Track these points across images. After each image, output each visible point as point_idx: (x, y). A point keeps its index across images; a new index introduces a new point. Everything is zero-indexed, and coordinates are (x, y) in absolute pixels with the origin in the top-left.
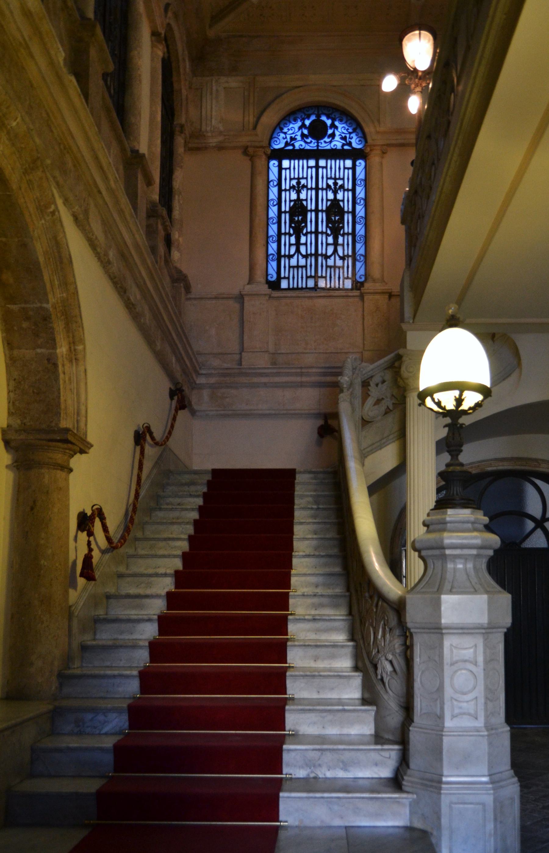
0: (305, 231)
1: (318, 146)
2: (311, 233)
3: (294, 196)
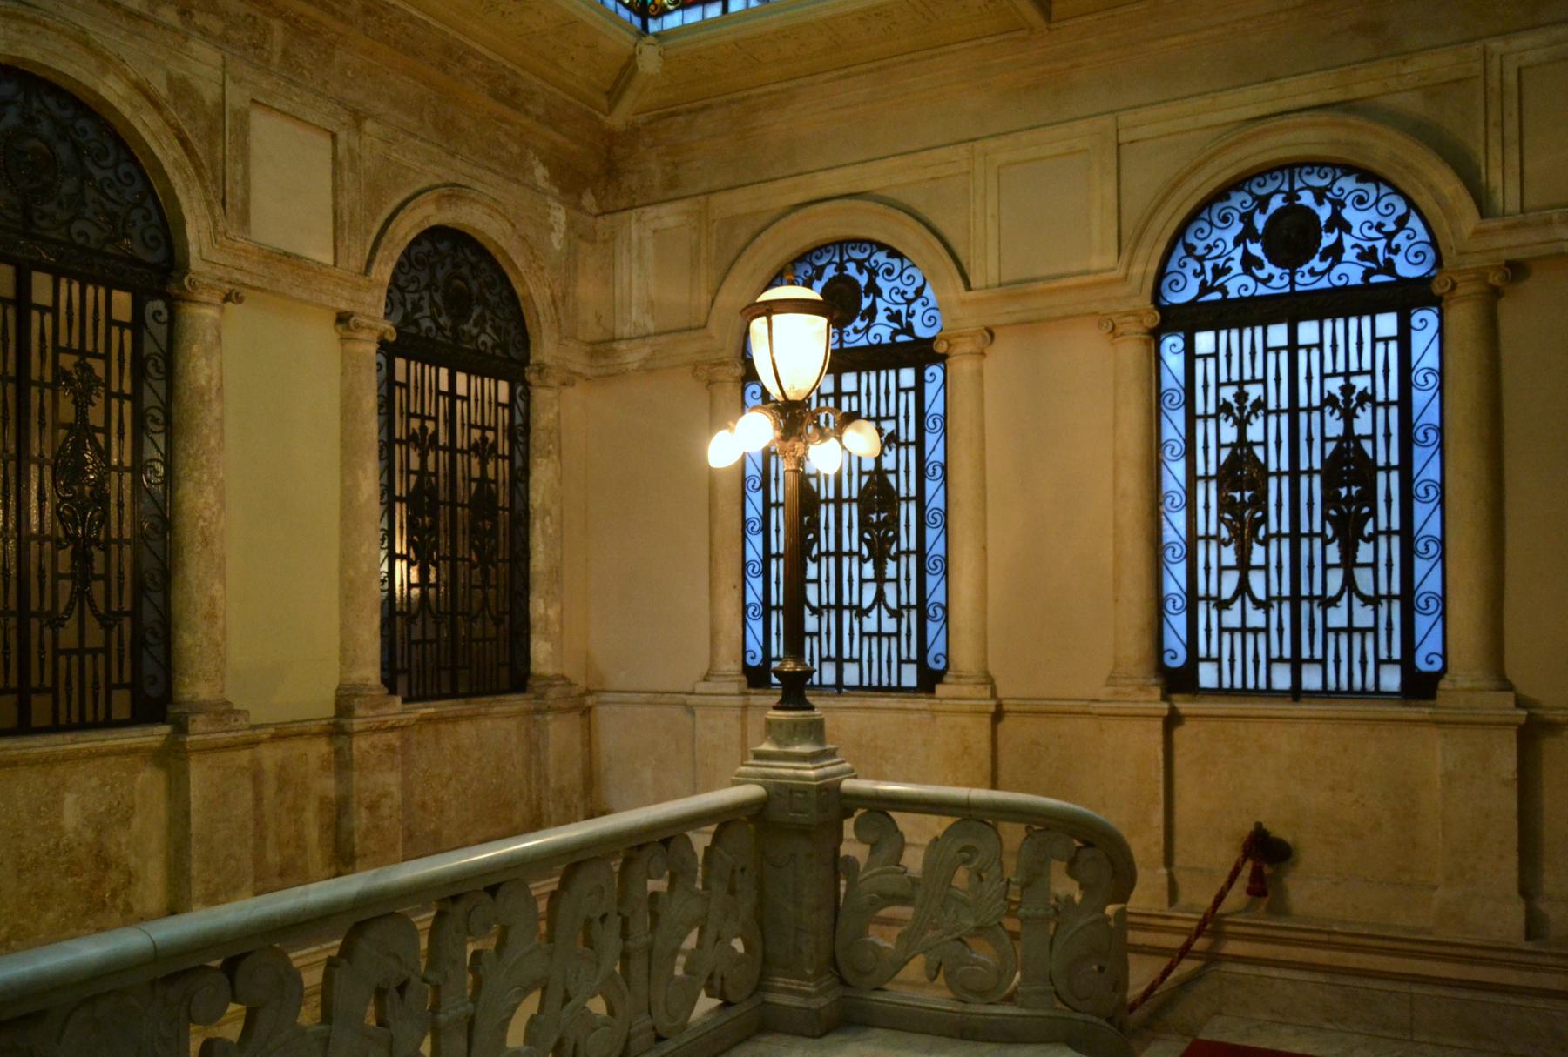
0: (815, 552)
1: (1292, 282)
2: (828, 554)
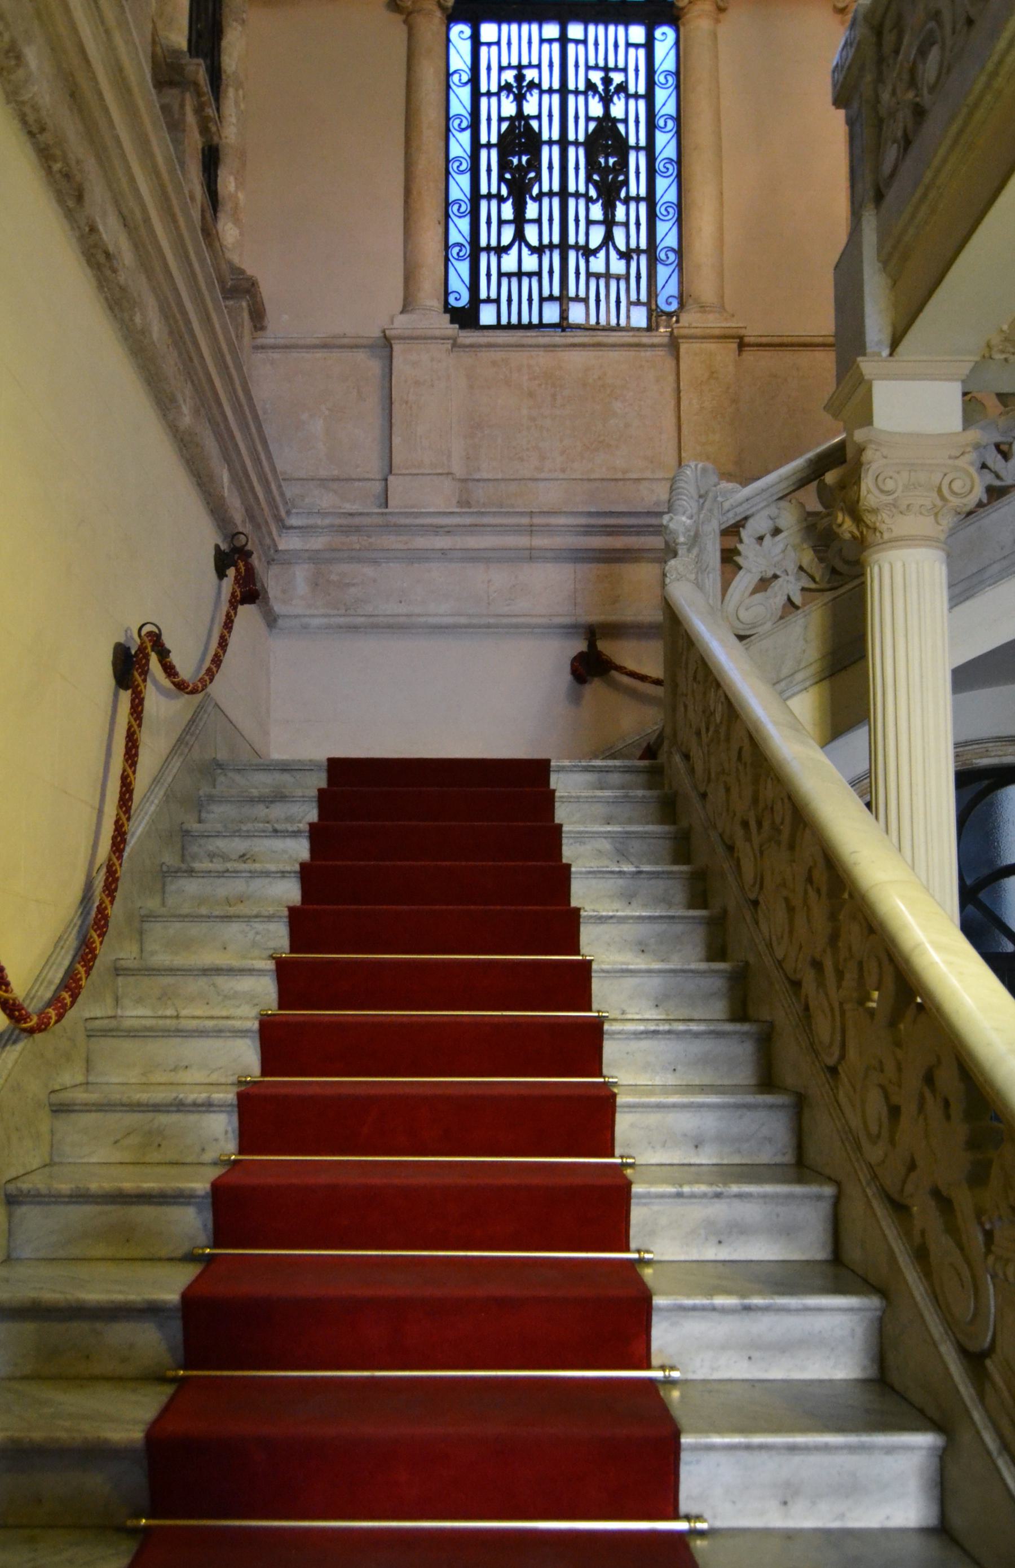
0: (535, 191)
2: (551, 194)
3: (509, 108)
